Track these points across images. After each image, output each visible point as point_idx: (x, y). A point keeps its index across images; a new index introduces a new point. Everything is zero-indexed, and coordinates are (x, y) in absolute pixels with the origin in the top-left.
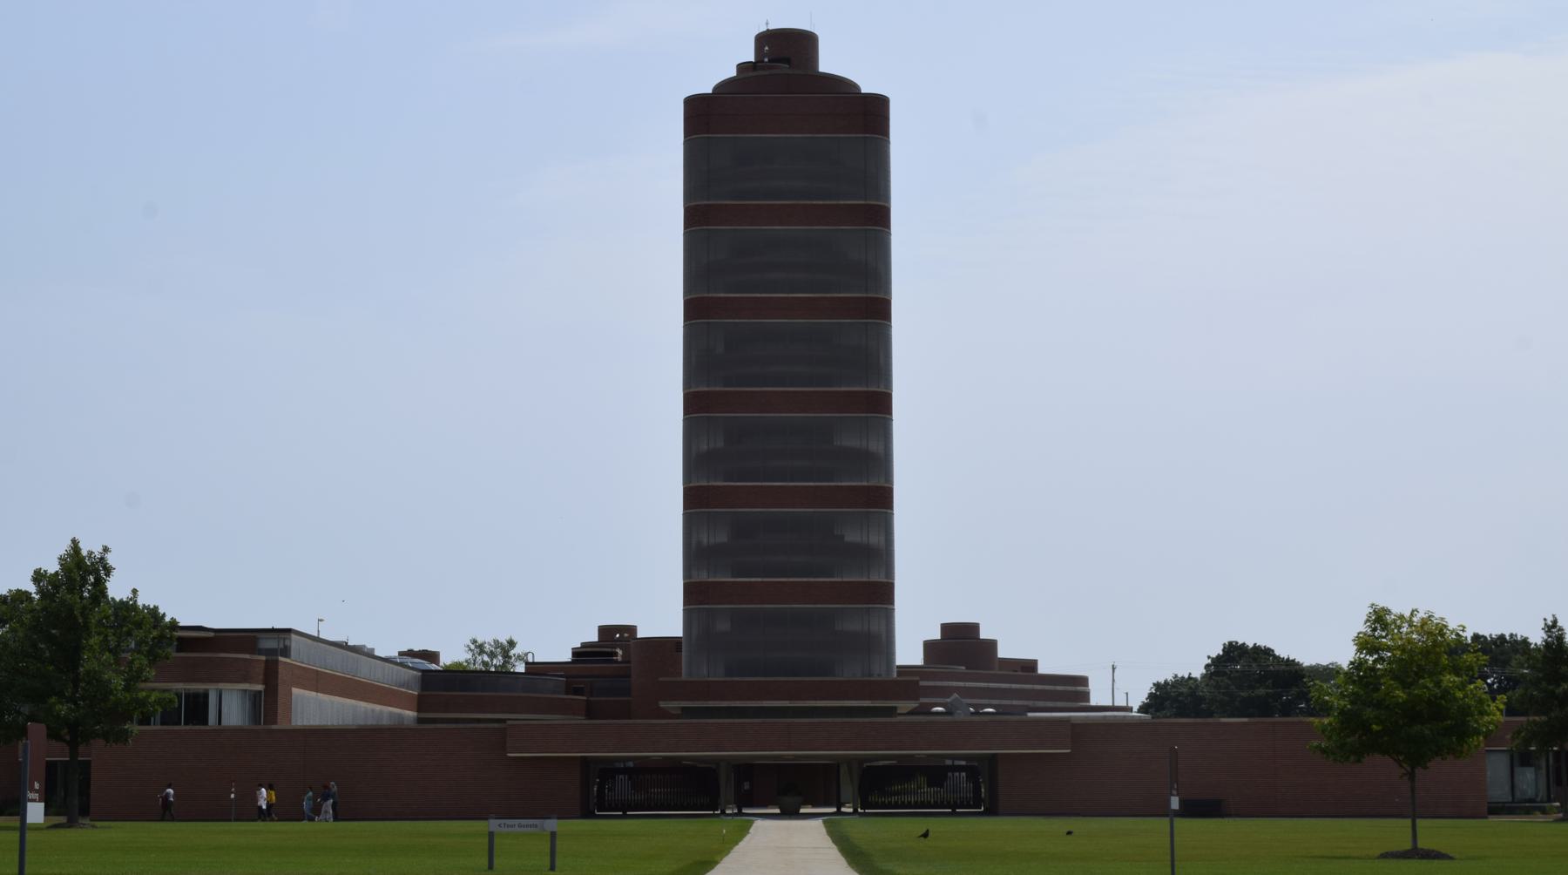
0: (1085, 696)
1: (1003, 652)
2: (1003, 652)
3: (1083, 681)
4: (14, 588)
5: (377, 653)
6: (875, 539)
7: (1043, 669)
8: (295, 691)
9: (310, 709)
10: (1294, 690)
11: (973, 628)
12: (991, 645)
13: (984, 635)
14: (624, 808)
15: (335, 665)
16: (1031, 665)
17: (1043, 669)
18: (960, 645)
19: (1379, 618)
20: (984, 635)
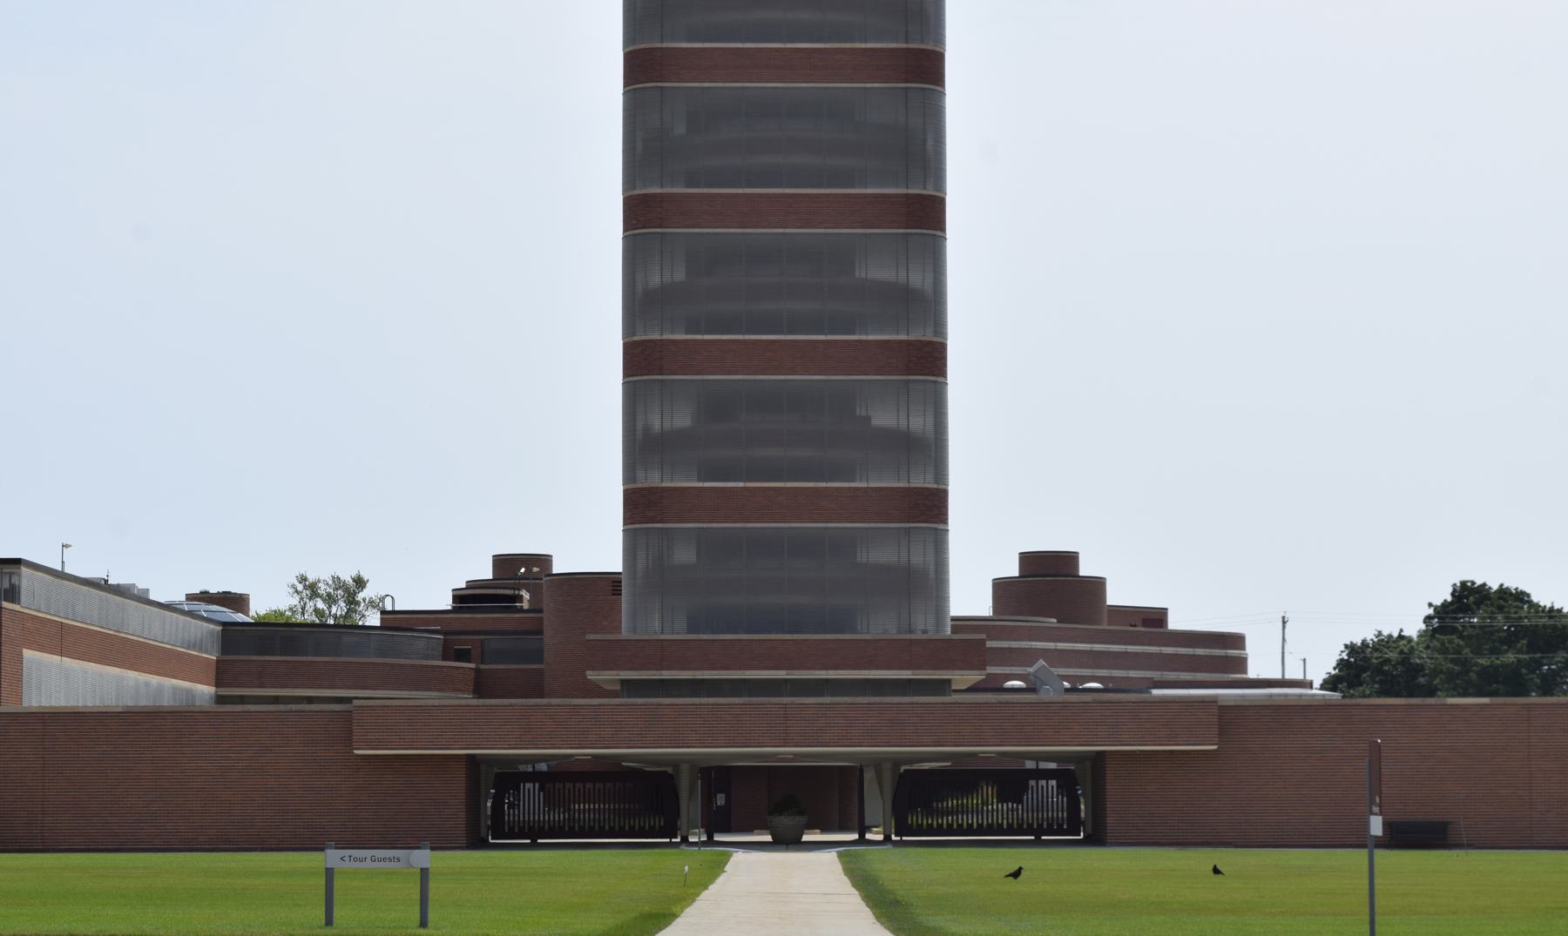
1: (1116, 596)
2: (1116, 596)
3: (1237, 641)
7: (1174, 623)
8: (28, 654)
11: (1065, 562)
16: (1156, 618)
17: (1174, 623)
18: (1049, 585)
20: (1085, 570)
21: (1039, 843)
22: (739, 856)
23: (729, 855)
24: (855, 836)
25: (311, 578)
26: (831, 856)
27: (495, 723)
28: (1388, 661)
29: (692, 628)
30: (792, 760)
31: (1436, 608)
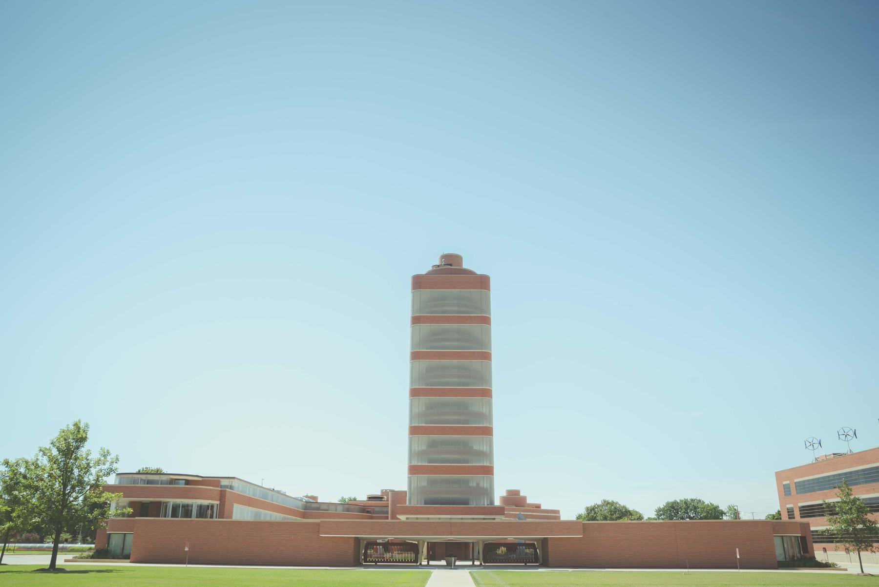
0: (559, 518)
1: (529, 501)
2: (529, 501)
3: (557, 512)
4: (347, 497)
5: (165, 471)
6: (485, 449)
7: (543, 507)
8: (235, 505)
9: (241, 513)
10: (64, 524)
11: (516, 493)
12: (524, 498)
13: (521, 494)
14: (378, 563)
15: (249, 493)
16: (538, 506)
17: (543, 507)
18: (514, 499)
19: (779, 475)
20: (521, 494)
21: (376, 566)
22: (435, 572)
23: (430, 573)
24: (470, 563)
25: (12, 461)
26: (466, 572)
27: (365, 536)
28: (32, 512)
29: (426, 503)
30: (20, 549)
31: (452, 505)
